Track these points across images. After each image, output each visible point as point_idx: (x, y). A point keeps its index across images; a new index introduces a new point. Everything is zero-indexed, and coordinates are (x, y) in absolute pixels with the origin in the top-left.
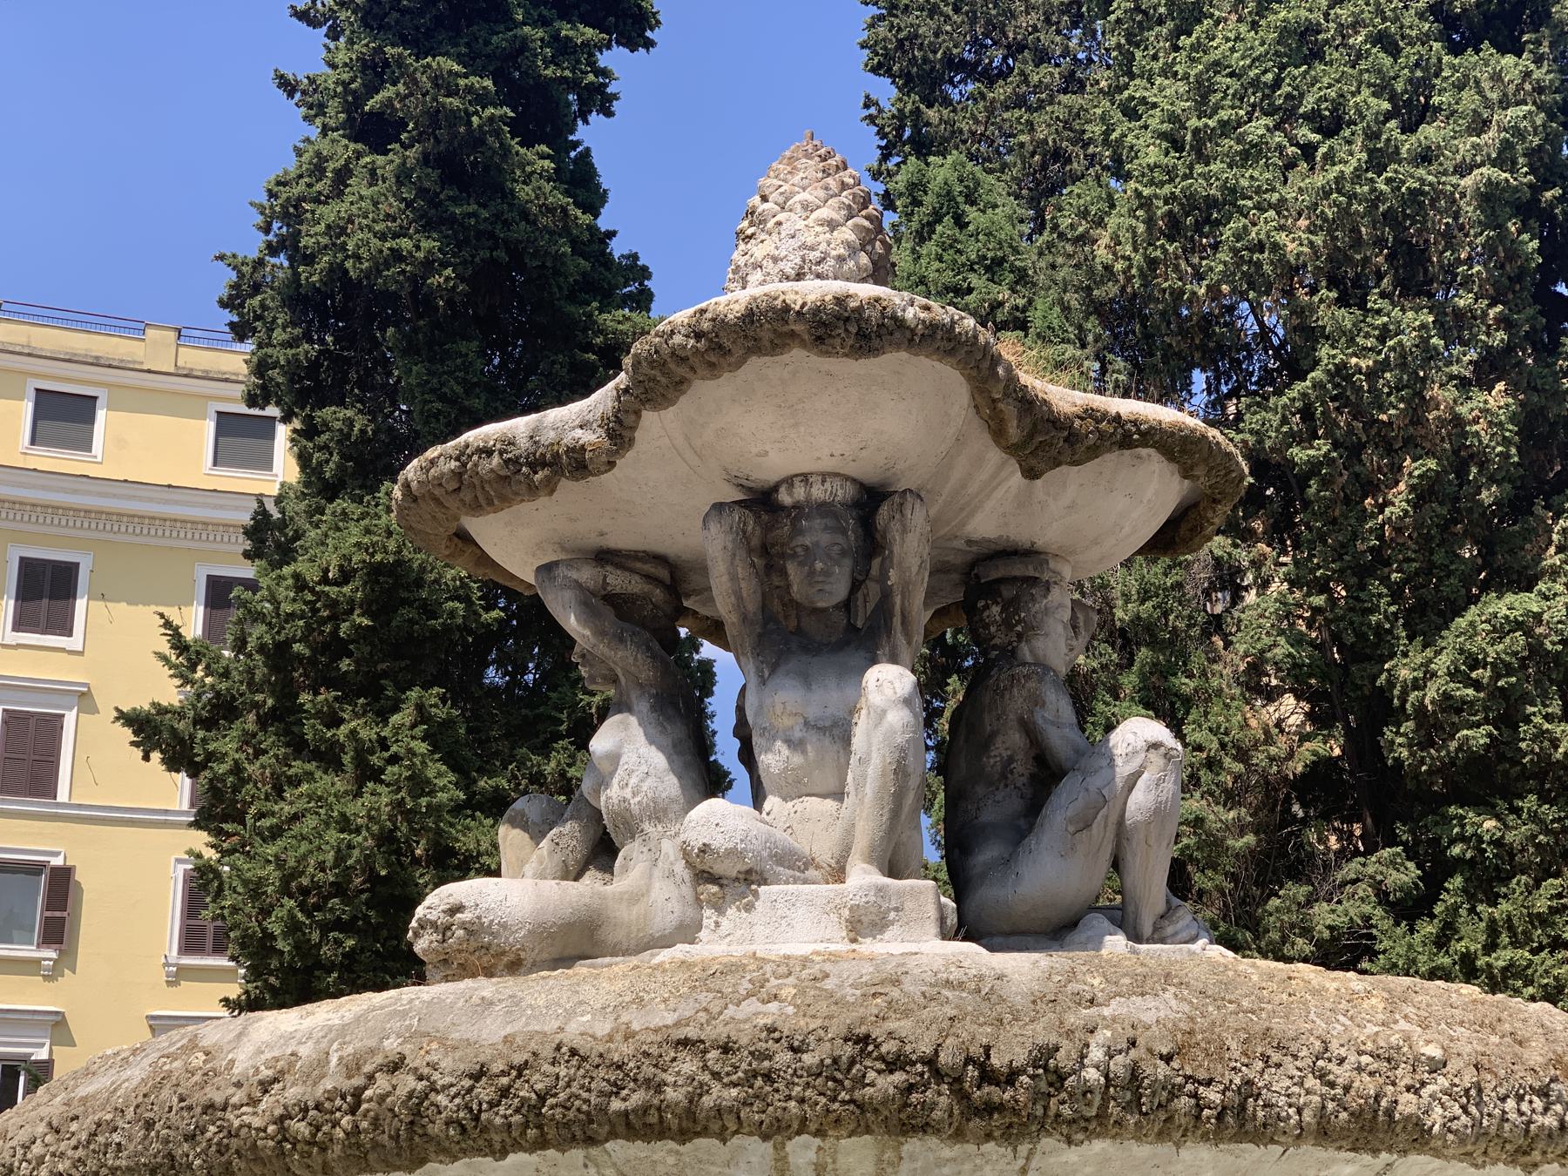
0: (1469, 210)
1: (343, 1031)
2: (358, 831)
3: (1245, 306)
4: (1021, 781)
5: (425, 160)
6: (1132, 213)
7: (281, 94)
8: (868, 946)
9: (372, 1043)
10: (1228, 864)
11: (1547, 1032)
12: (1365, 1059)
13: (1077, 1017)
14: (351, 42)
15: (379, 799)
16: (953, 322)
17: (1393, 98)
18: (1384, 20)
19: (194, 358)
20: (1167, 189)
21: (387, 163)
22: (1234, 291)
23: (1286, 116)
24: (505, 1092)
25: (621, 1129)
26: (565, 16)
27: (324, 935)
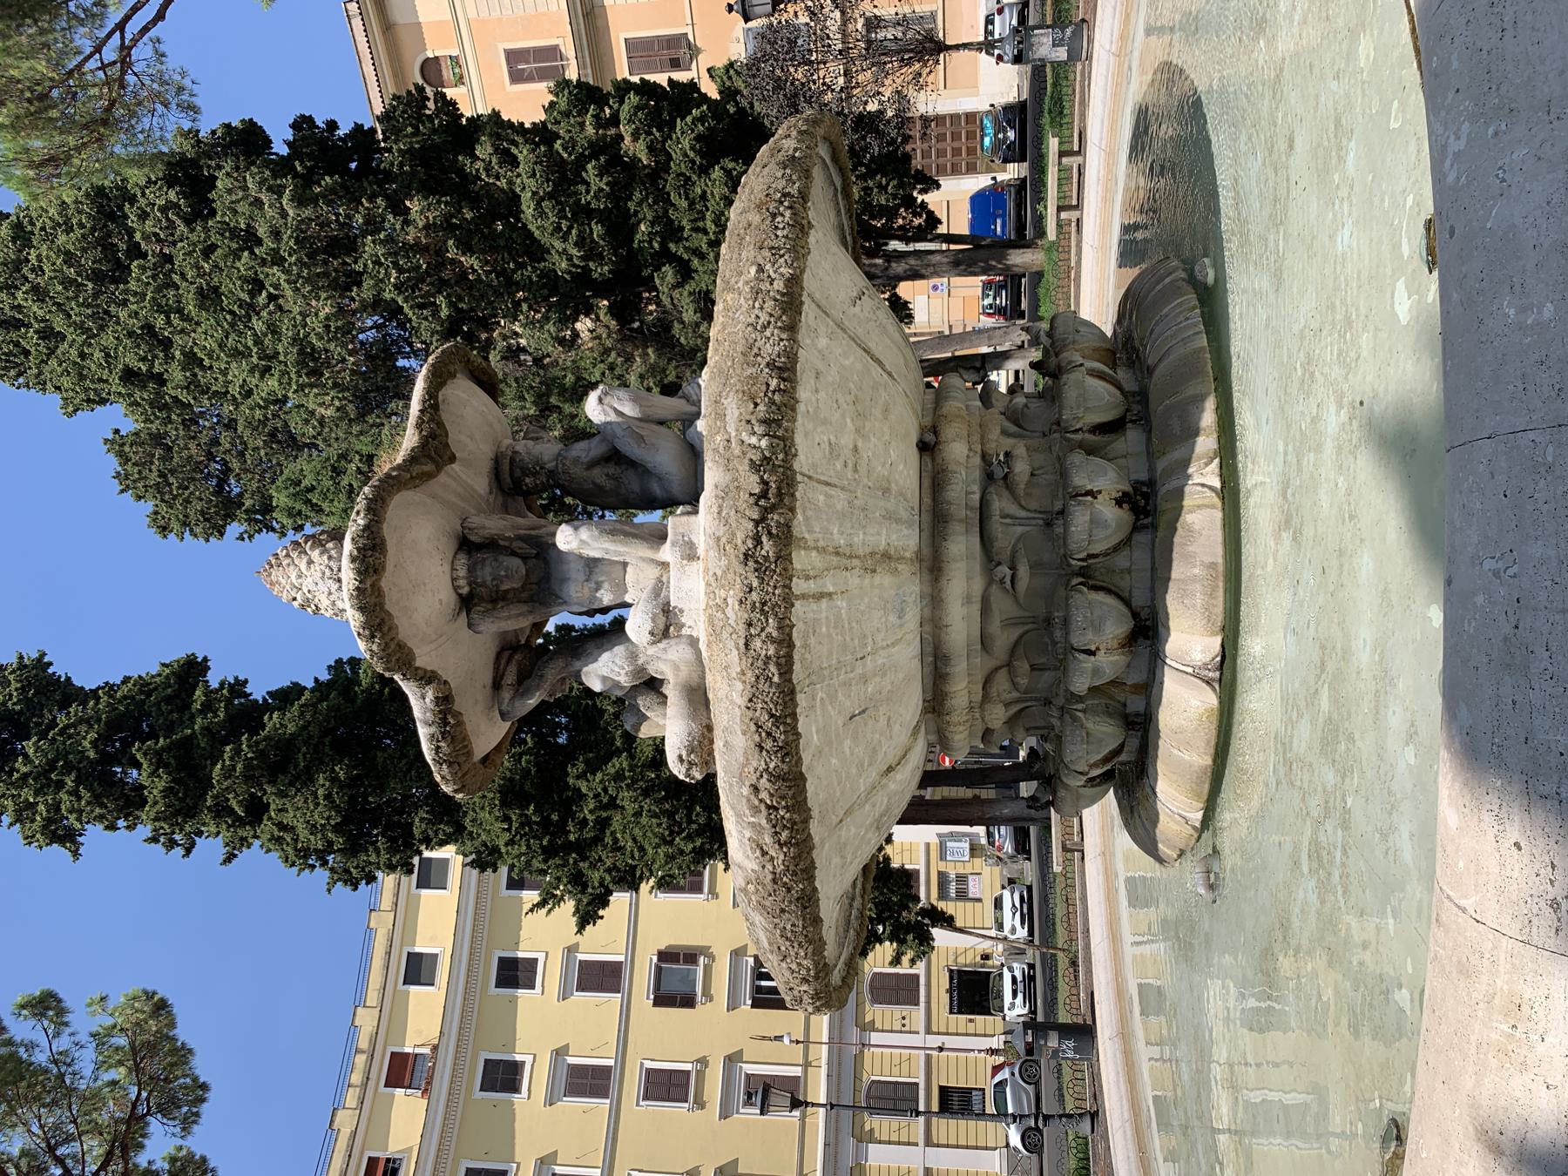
0: (308, 212)
1: (738, 815)
2: (641, 807)
3: (360, 336)
4: (619, 471)
5: (272, 782)
6: (307, 395)
7: (235, 861)
8: (701, 551)
9: (744, 801)
10: (663, 363)
11: (744, 211)
12: (757, 305)
13: (736, 449)
14: (204, 824)
15: (626, 797)
16: (366, 498)
17: (242, 250)
18: (195, 251)
19: (386, 901)
20: (293, 376)
21: (275, 803)
22: (352, 342)
23: (251, 309)
24: (769, 734)
25: (787, 676)
26: (188, 706)
27: (694, 822)
